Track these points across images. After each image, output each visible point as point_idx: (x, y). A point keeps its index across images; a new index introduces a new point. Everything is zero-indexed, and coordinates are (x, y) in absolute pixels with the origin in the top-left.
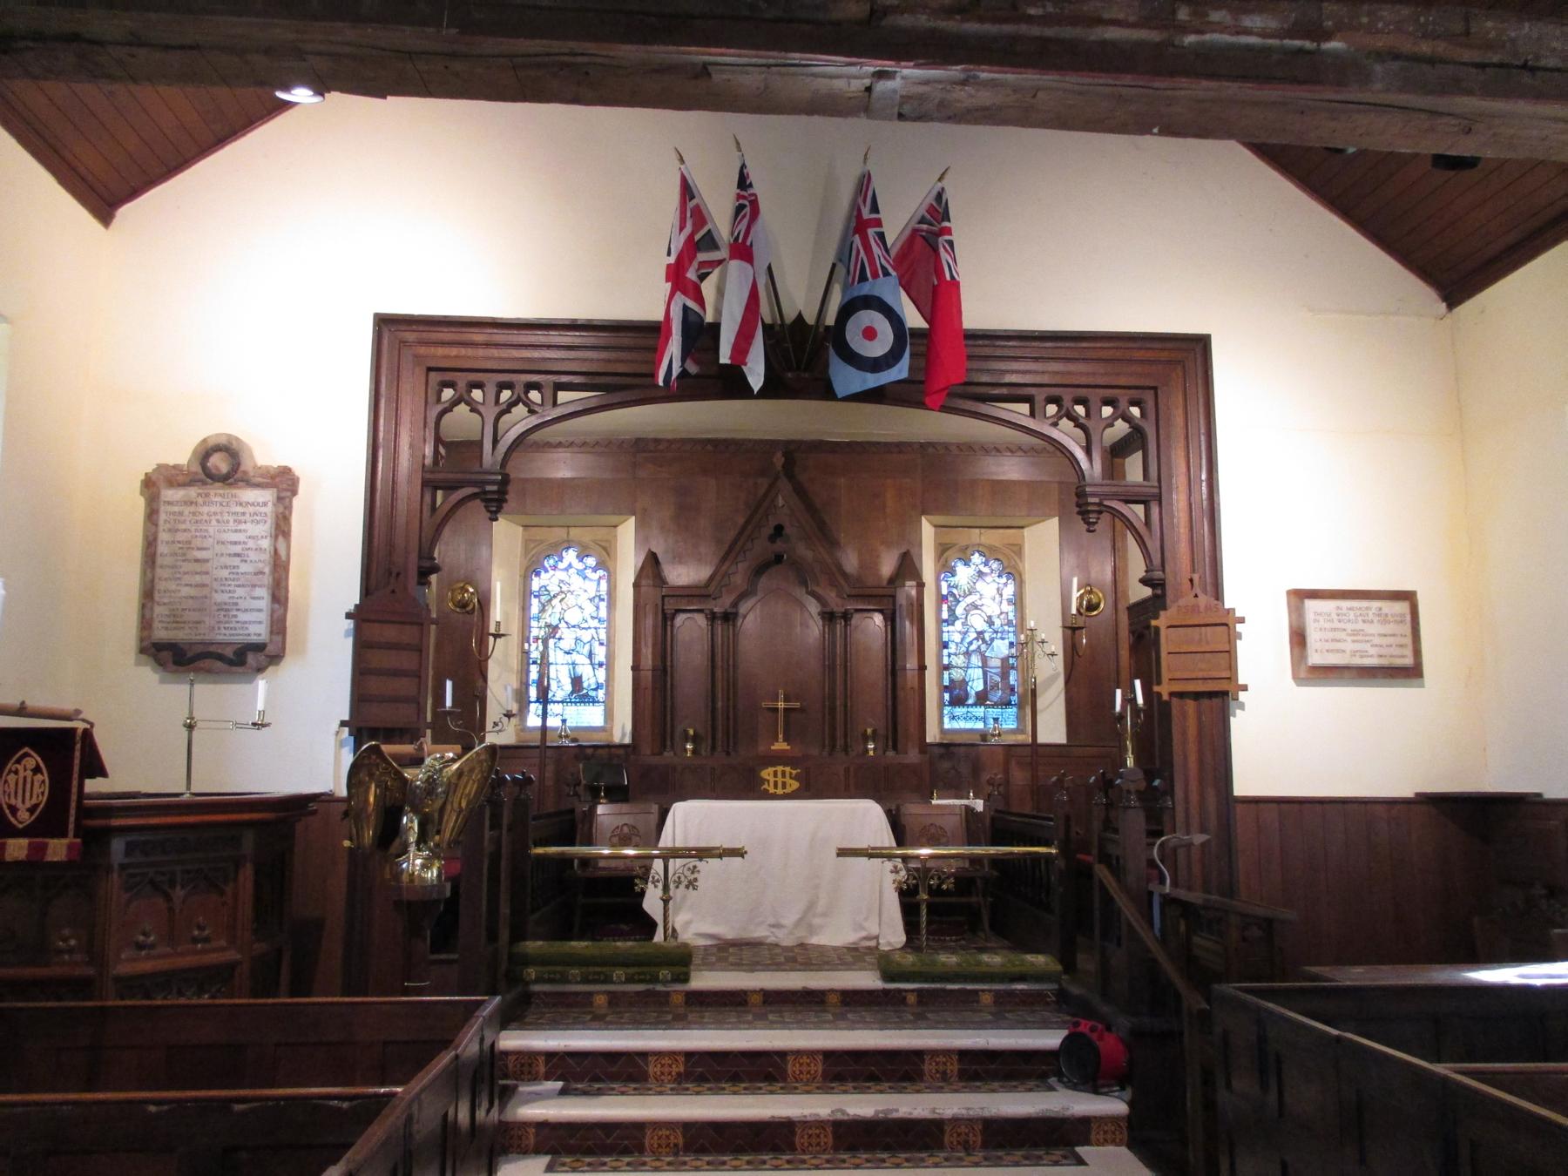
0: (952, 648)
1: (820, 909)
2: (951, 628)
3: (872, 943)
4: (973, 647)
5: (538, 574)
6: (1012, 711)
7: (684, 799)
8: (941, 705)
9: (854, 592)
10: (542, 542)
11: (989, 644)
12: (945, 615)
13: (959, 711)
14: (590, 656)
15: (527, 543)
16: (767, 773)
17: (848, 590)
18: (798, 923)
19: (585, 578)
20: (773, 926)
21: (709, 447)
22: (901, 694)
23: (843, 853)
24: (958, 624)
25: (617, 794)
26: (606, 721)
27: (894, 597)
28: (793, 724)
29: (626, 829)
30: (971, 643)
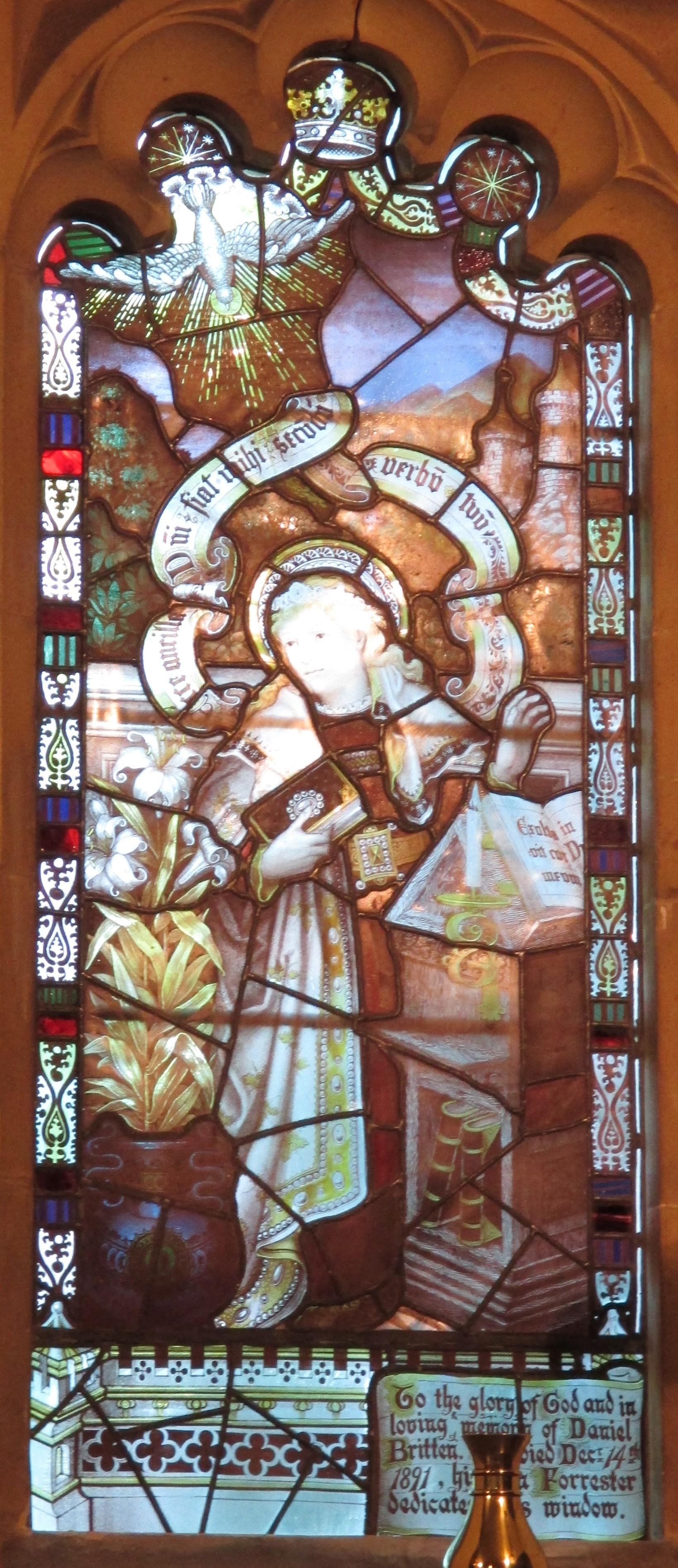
2: (108, 680)
4: (291, 848)
6: (606, 1396)
11: (424, 826)
13: (160, 1386)
24: (170, 660)
30: (269, 815)
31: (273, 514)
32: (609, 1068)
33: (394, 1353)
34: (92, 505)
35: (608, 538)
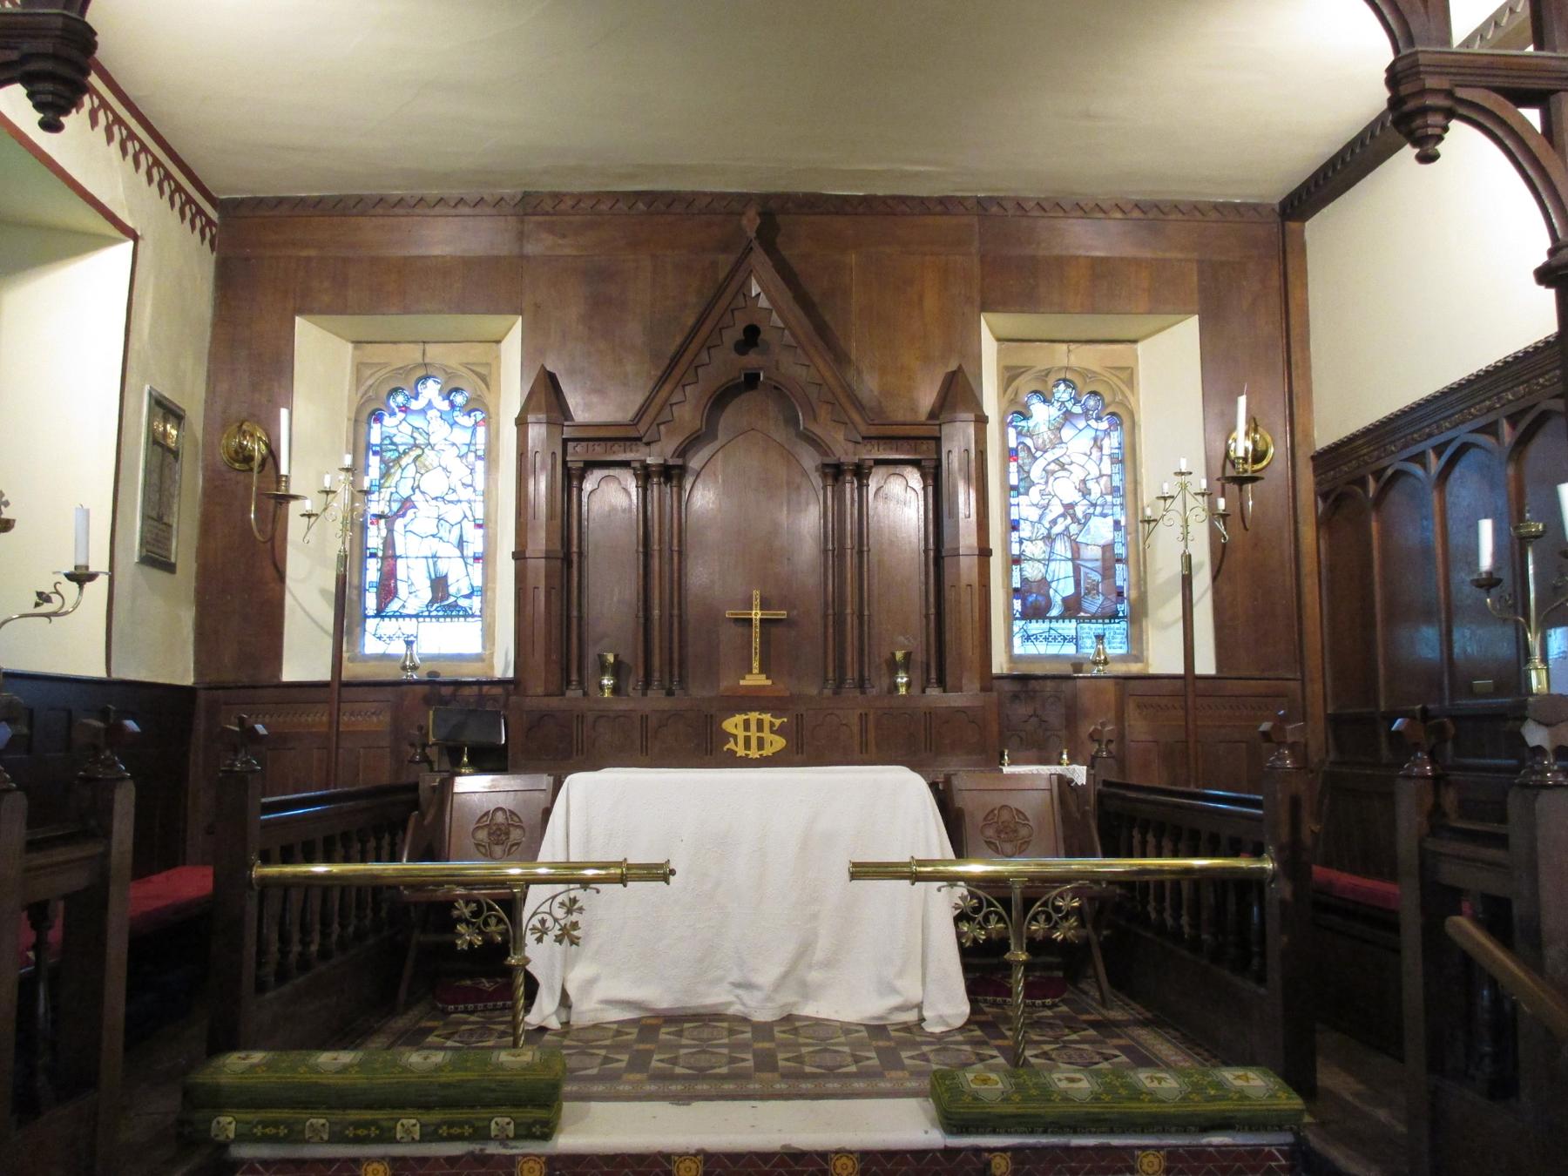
0: (1025, 530)
1: (819, 955)
2: (1022, 499)
3: (911, 1017)
4: (1057, 529)
5: (379, 419)
7: (593, 763)
8: (1010, 618)
9: (873, 431)
10: (386, 365)
11: (1083, 523)
12: (1014, 480)
13: (1035, 627)
14: (461, 543)
15: (359, 368)
16: (733, 724)
17: (863, 428)
18: (779, 985)
19: (453, 424)
20: (738, 985)
21: (641, 206)
22: (949, 594)
23: (861, 871)
24: (1034, 491)
25: (489, 760)
26: (484, 647)
27: (938, 440)
28: (660, 475)
29: (500, 817)
30: (1054, 522)
31: (1053, 467)
32: (1119, 567)
33: (1081, 620)
34: (1019, 467)
35: (1117, 467)
